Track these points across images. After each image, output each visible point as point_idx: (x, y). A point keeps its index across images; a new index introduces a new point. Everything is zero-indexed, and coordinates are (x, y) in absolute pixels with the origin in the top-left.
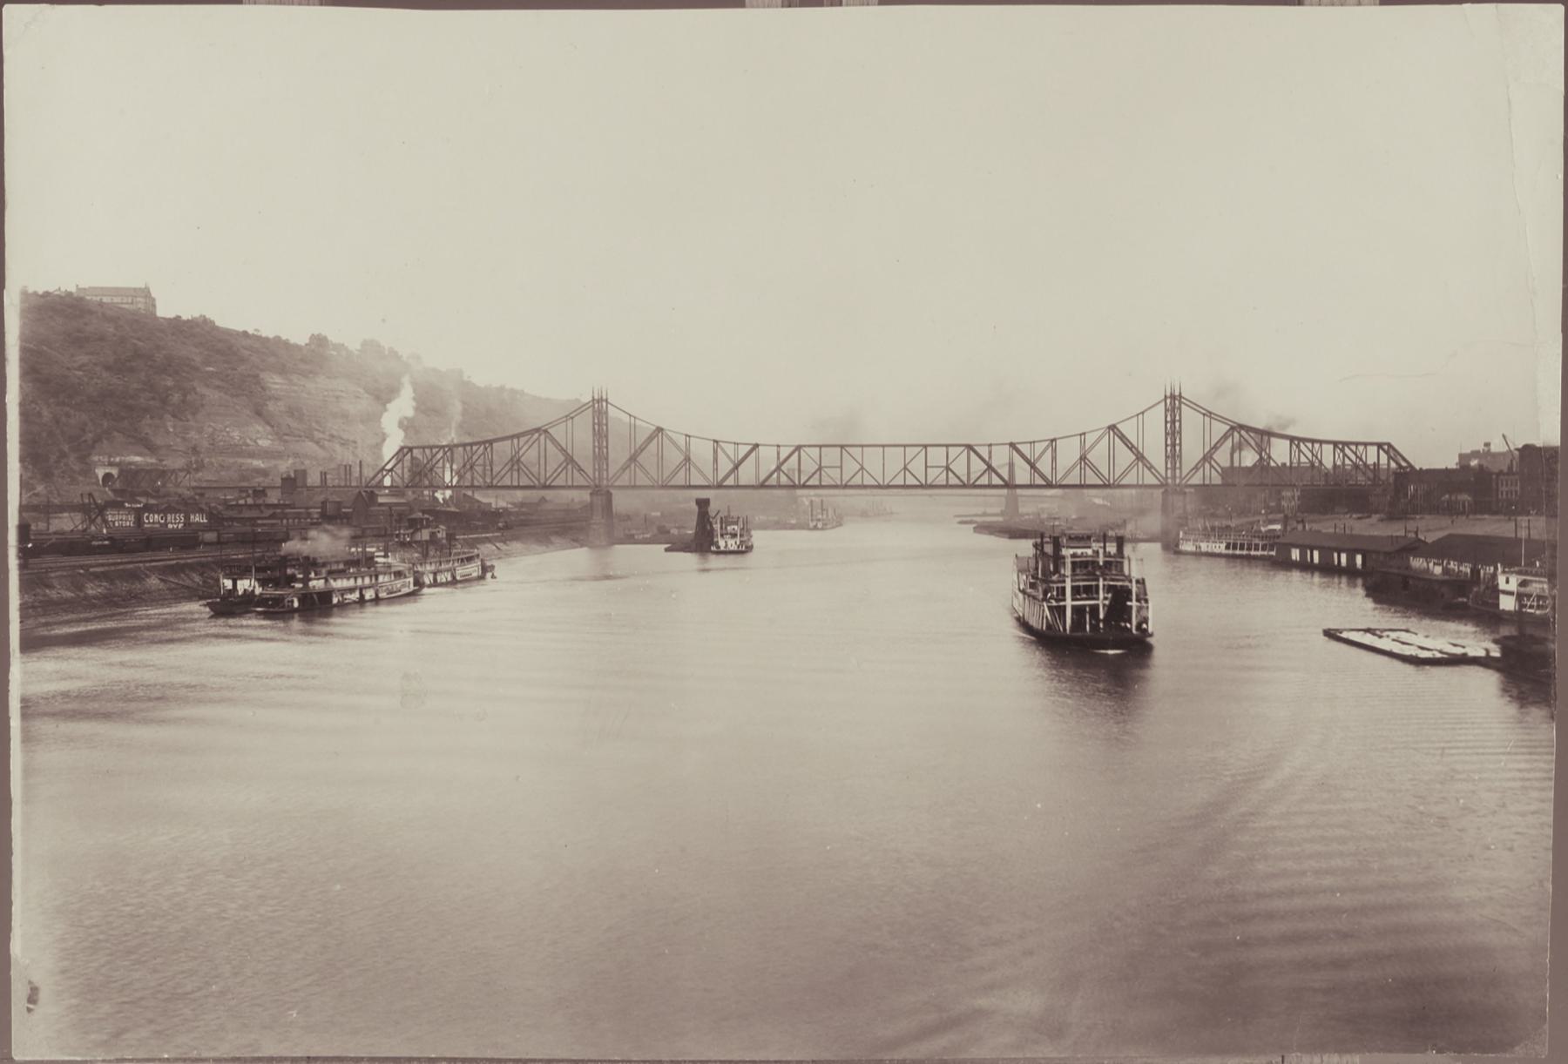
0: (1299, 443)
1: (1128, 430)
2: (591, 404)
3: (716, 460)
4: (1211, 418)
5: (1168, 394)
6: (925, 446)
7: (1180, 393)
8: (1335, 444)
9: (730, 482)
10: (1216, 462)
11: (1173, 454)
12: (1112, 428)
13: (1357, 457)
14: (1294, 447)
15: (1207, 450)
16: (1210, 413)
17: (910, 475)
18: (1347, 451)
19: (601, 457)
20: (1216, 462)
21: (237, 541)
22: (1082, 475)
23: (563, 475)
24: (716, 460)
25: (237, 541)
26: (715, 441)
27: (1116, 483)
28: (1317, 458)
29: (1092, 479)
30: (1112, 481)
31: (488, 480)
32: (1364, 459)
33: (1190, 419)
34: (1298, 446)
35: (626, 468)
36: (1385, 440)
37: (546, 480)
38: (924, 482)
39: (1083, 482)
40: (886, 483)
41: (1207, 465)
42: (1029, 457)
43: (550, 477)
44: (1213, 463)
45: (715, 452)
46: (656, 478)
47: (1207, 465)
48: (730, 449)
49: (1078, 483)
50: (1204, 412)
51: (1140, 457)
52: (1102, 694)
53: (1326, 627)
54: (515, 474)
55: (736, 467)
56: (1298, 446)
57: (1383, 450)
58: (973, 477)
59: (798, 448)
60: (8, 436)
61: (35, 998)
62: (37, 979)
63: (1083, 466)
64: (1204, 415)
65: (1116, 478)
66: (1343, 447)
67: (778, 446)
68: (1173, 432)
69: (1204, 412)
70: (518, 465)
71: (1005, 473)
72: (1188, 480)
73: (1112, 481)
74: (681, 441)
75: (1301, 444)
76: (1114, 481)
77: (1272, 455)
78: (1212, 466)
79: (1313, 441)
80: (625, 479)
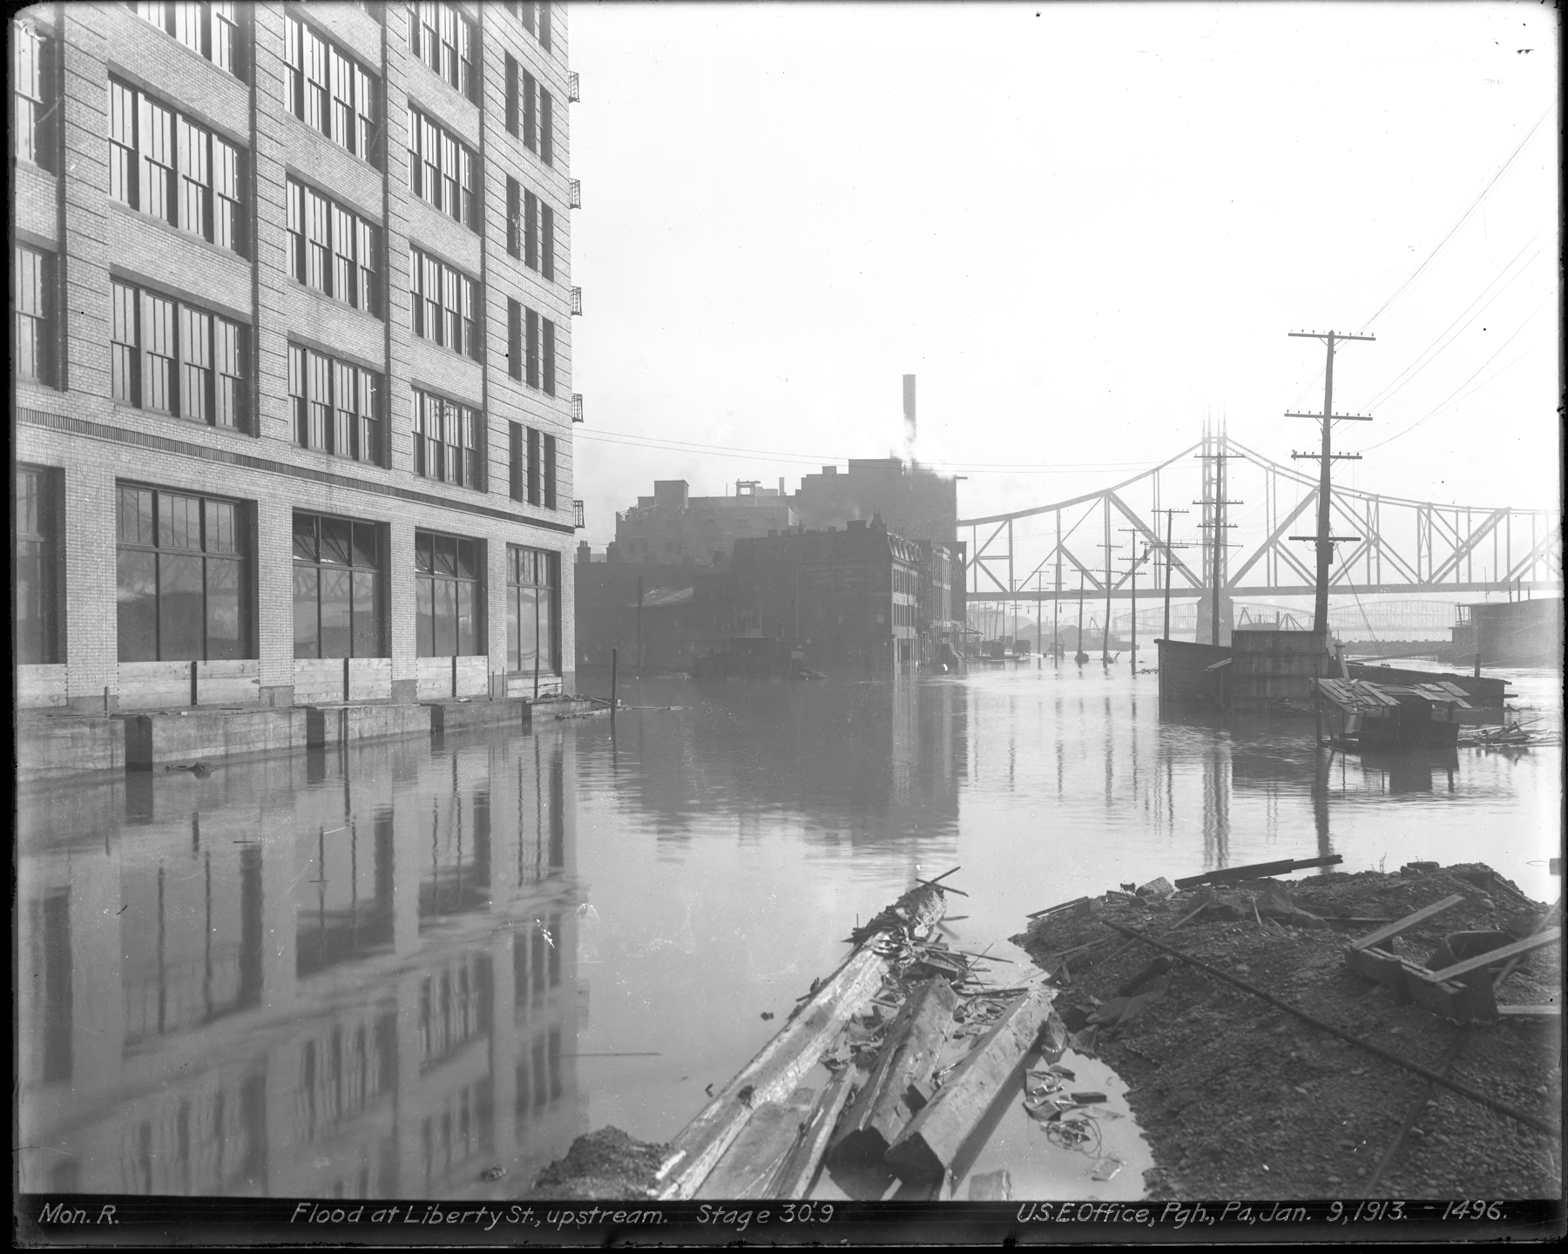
0: (1429, 513)
2: (1271, 474)
4: (1275, 472)
6: (1008, 518)
7: (1225, 433)
12: (1109, 496)
14: (1424, 519)
15: (1272, 532)
16: (1274, 465)
21: (1518, 711)
22: (1272, 571)
25: (1518, 711)
28: (1372, 530)
32: (1375, 530)
37: (1431, 577)
39: (1272, 585)
40: (1499, 580)
41: (1271, 550)
43: (1436, 573)
44: (1278, 547)
47: (1271, 550)
50: (1267, 464)
52: (31, 175)
53: (1012, 934)
61: (487, 1179)
62: (413, 201)
63: (1476, 537)
64: (1267, 469)
69: (1267, 464)
70: (1377, 546)
71: (1101, 577)
72: (1336, 582)
73: (1425, 577)
78: (1276, 551)
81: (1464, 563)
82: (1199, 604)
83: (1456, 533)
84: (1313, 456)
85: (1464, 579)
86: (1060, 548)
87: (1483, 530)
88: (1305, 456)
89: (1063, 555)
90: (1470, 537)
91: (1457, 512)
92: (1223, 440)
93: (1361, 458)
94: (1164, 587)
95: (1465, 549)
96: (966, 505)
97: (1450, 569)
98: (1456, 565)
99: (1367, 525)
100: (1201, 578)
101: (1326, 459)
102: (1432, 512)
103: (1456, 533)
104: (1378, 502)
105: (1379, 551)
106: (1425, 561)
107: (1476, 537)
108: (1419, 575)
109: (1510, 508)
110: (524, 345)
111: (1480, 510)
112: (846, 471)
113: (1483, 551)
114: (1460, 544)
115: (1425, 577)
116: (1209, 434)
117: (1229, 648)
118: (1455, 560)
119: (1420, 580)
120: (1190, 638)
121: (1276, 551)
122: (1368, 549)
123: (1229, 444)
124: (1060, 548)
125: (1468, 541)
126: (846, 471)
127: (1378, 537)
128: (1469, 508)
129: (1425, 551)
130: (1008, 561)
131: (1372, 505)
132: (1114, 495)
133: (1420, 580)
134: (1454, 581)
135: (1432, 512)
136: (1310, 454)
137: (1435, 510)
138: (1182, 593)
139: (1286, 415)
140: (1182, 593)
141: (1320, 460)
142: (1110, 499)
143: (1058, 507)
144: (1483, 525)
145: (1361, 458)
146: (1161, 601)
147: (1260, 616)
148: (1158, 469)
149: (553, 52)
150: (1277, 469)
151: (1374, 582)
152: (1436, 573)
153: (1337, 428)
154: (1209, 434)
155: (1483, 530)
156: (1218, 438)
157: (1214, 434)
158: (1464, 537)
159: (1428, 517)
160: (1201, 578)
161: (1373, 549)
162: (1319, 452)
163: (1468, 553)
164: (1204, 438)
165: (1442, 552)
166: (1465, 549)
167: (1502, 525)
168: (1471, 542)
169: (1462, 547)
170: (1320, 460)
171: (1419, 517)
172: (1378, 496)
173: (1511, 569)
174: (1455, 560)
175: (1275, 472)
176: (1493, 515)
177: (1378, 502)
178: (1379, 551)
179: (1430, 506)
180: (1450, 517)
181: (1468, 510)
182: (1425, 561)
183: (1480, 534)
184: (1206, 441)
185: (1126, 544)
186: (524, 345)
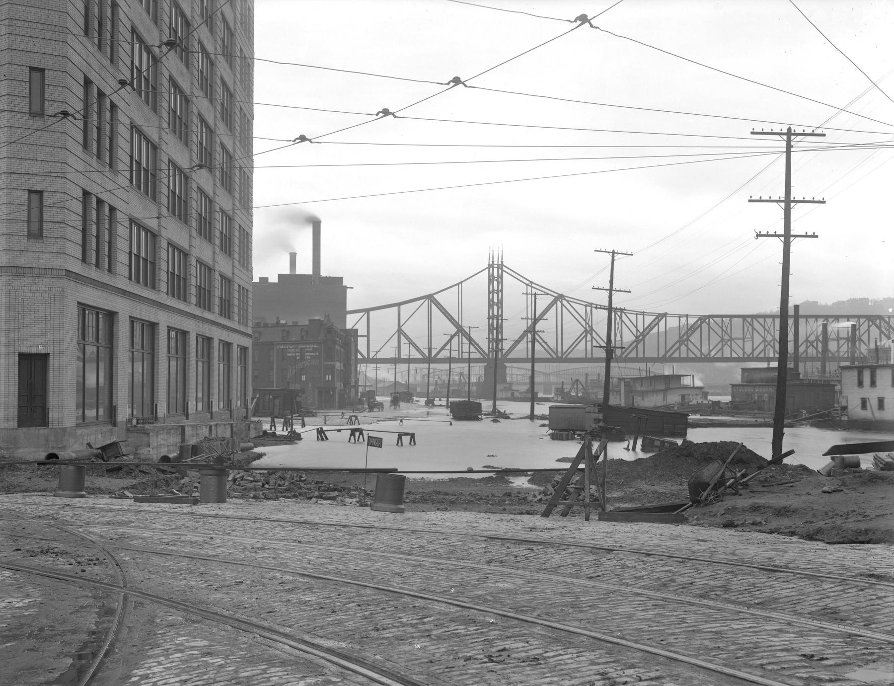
0: (621, 315)
1: (448, 300)
4: (532, 287)
6: (367, 311)
7: (502, 262)
8: (744, 317)
12: (430, 298)
13: (765, 329)
16: (532, 282)
18: (756, 325)
31: (705, 350)
33: (512, 289)
38: (366, 356)
40: (660, 356)
42: (457, 320)
43: (669, 350)
46: (553, 345)
50: (527, 282)
54: (683, 348)
58: (437, 344)
60: (728, 440)
63: (648, 330)
64: (527, 285)
65: (565, 350)
66: (752, 320)
67: (613, 253)
68: (495, 302)
70: (591, 335)
73: (560, 355)
76: (563, 354)
77: (594, 328)
81: (640, 346)
82: (485, 367)
83: (636, 327)
84: (775, 235)
85: (641, 355)
86: (400, 331)
87: (652, 326)
88: (768, 235)
89: (402, 337)
90: (644, 330)
91: (637, 314)
92: (501, 266)
93: (817, 237)
94: (530, 356)
95: (641, 337)
96: (353, 301)
98: (636, 347)
99: (585, 321)
100: (487, 351)
101: (787, 237)
102: (623, 314)
103: (636, 327)
104: (592, 307)
105: (592, 337)
107: (648, 330)
109: (666, 313)
111: (650, 314)
112: (276, 281)
114: (639, 334)
115: (560, 355)
116: (493, 262)
118: (635, 343)
119: (702, 353)
122: (586, 336)
123: (504, 269)
124: (400, 331)
125: (643, 332)
126: (276, 281)
127: (592, 329)
128: (644, 312)
130: (366, 339)
131: (589, 309)
132: (434, 299)
133: (702, 353)
134: (678, 356)
135: (623, 314)
136: (765, 233)
137: (625, 313)
138: (477, 361)
139: (750, 201)
140: (477, 361)
141: (782, 239)
142: (432, 301)
143: (399, 305)
144: (651, 323)
145: (817, 237)
146: (529, 366)
147: (586, 375)
148: (461, 282)
149: (83, 76)
150: (533, 285)
152: (669, 350)
153: (797, 211)
154: (493, 262)
155: (652, 326)
156: (498, 265)
157: (496, 262)
158: (641, 330)
159: (621, 317)
160: (487, 351)
161: (589, 336)
162: (781, 231)
163: (643, 339)
164: (489, 264)
166: (641, 337)
168: (645, 333)
169: (640, 336)
170: (782, 239)
173: (678, 351)
174: (635, 343)
175: (532, 287)
176: (657, 317)
177: (592, 307)
178: (592, 337)
180: (633, 317)
181: (643, 313)
183: (650, 327)
184: (491, 266)
185: (443, 328)
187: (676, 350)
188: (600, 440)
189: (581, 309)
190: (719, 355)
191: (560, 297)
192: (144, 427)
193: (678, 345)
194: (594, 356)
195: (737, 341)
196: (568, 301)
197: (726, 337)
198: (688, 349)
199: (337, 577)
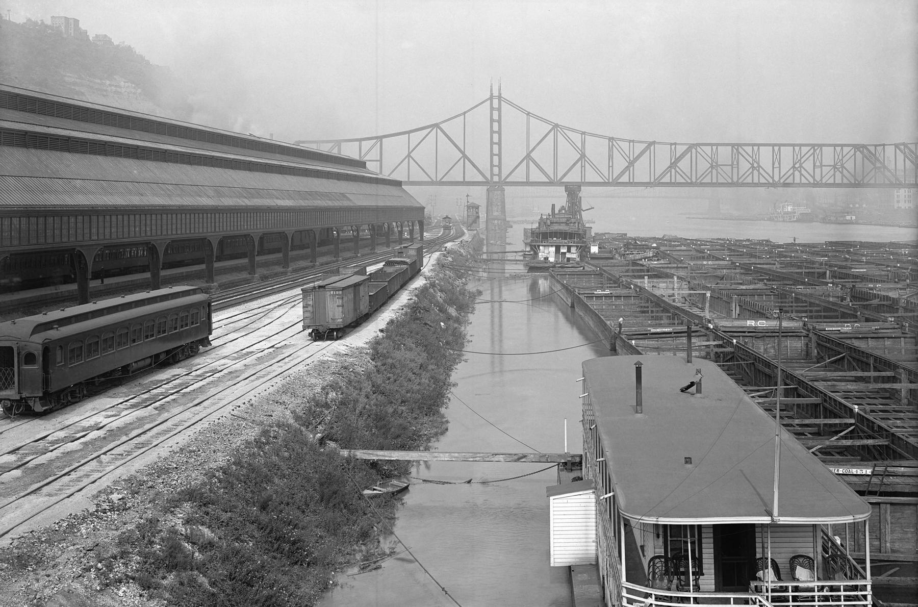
1: (454, 129)
3: (611, 157)
5: (496, 93)
6: (380, 138)
7: (500, 94)
9: (625, 179)
10: (749, 162)
11: (496, 154)
12: (436, 126)
14: (735, 151)
17: (740, 173)
19: (496, 154)
20: (749, 162)
23: (750, 178)
24: (611, 157)
26: (611, 139)
27: (740, 181)
29: (536, 176)
30: (776, 178)
33: (511, 118)
34: (737, 150)
35: (678, 158)
36: (901, 141)
41: (673, 171)
45: (610, 150)
47: (673, 171)
48: (624, 146)
49: (649, 181)
51: (465, 156)
55: (631, 163)
56: (737, 150)
57: (900, 150)
59: (691, 147)
73: (735, 179)
74: (577, 138)
75: (698, 148)
78: (676, 171)
79: (753, 145)
80: (519, 175)
97: (667, 173)
99: (752, 158)
106: (776, 170)
108: (773, 178)
110: (235, 298)
113: (684, 164)
117: (105, 278)
120: (77, 286)
121: (676, 171)
129: (776, 165)
133: (773, 180)
143: (409, 132)
151: (673, 181)
165: (620, 164)
167: (652, 148)
171: (732, 150)
172: (585, 132)
176: (649, 145)
179: (613, 138)
182: (776, 170)
184: (491, 98)
186: (235, 298)
187: (717, 175)
188: (149, 271)
189: (577, 138)
190: (831, 181)
191: (556, 126)
192: (484, 245)
193: (751, 170)
194: (466, 180)
195: (724, 168)
196: (561, 128)
197: (755, 165)
198: (801, 175)
199: (660, 326)
